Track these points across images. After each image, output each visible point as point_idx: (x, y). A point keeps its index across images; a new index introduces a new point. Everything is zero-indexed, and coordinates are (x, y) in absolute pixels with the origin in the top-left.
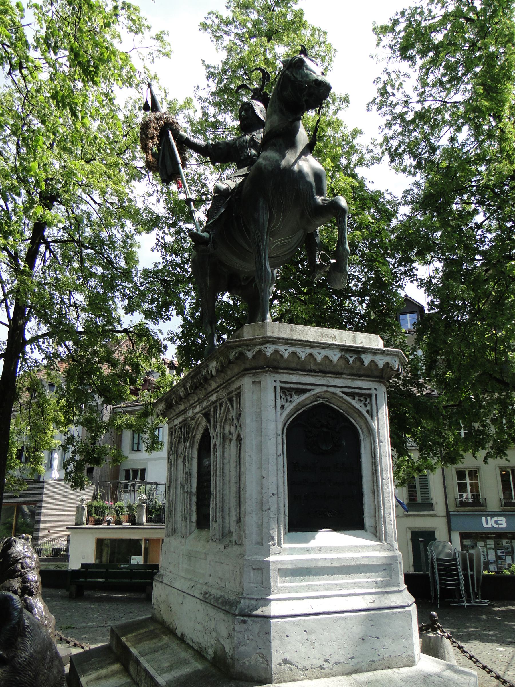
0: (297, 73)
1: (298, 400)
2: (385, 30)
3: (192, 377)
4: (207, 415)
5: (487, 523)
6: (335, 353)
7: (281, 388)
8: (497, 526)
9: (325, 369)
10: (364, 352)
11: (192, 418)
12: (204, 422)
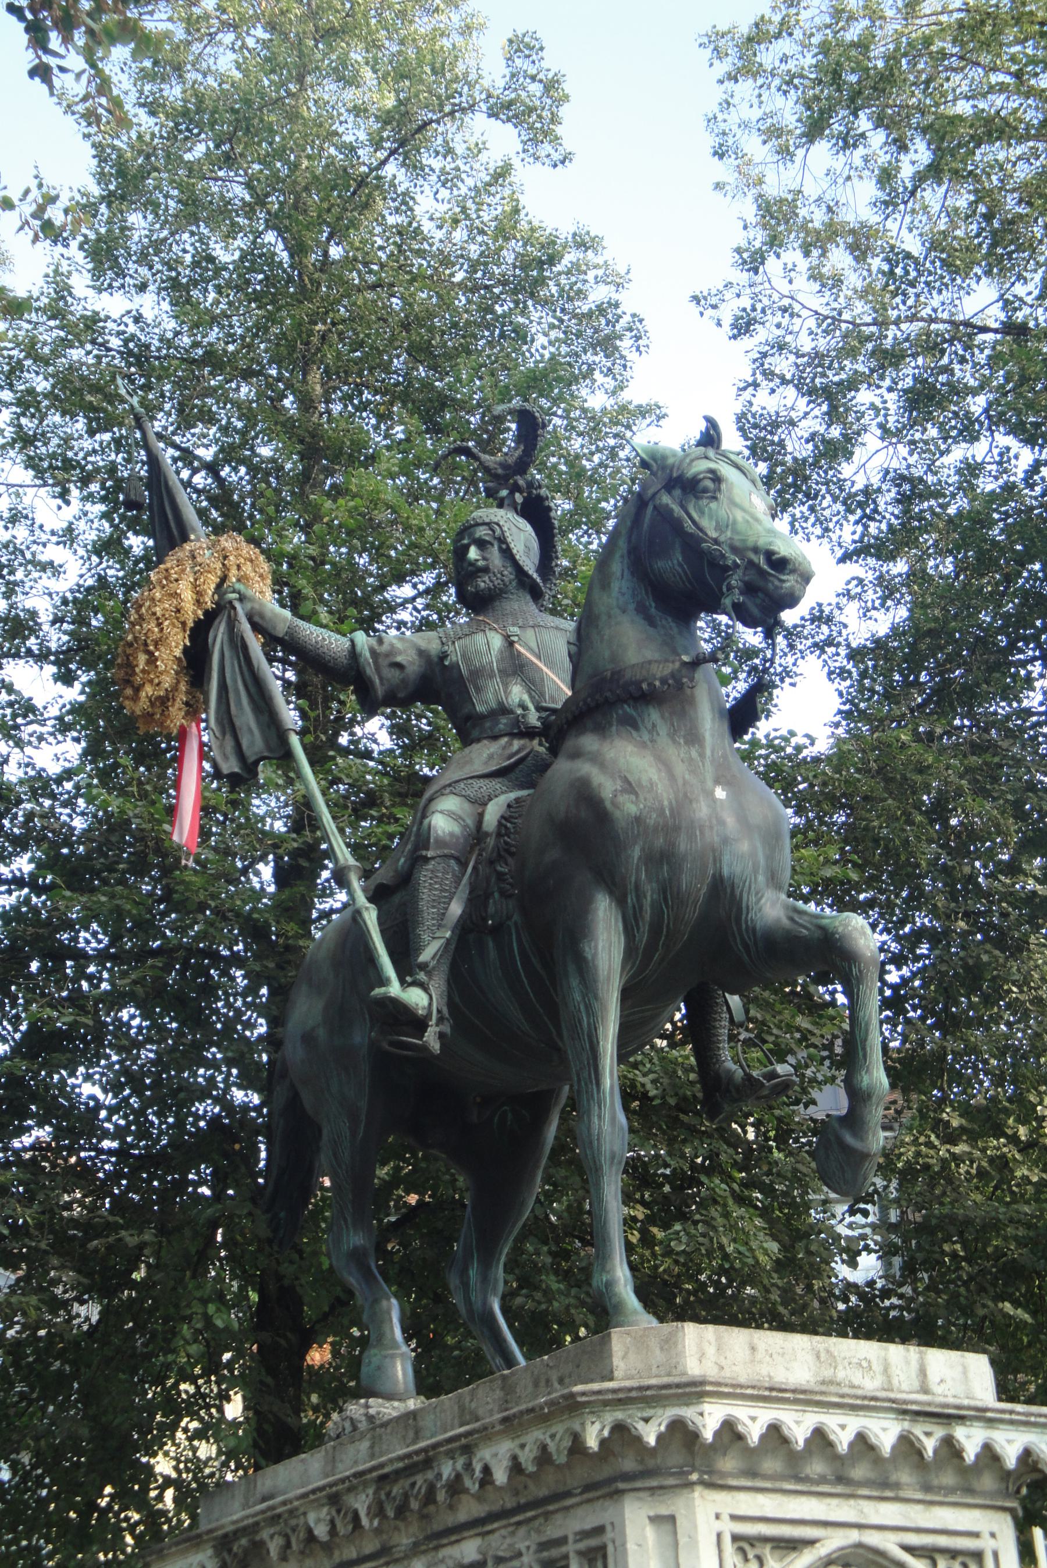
0: (702, 513)
2: (760, 35)
3: (383, 1478)
6: (886, 1423)
7: (736, 1538)
10: (961, 1419)
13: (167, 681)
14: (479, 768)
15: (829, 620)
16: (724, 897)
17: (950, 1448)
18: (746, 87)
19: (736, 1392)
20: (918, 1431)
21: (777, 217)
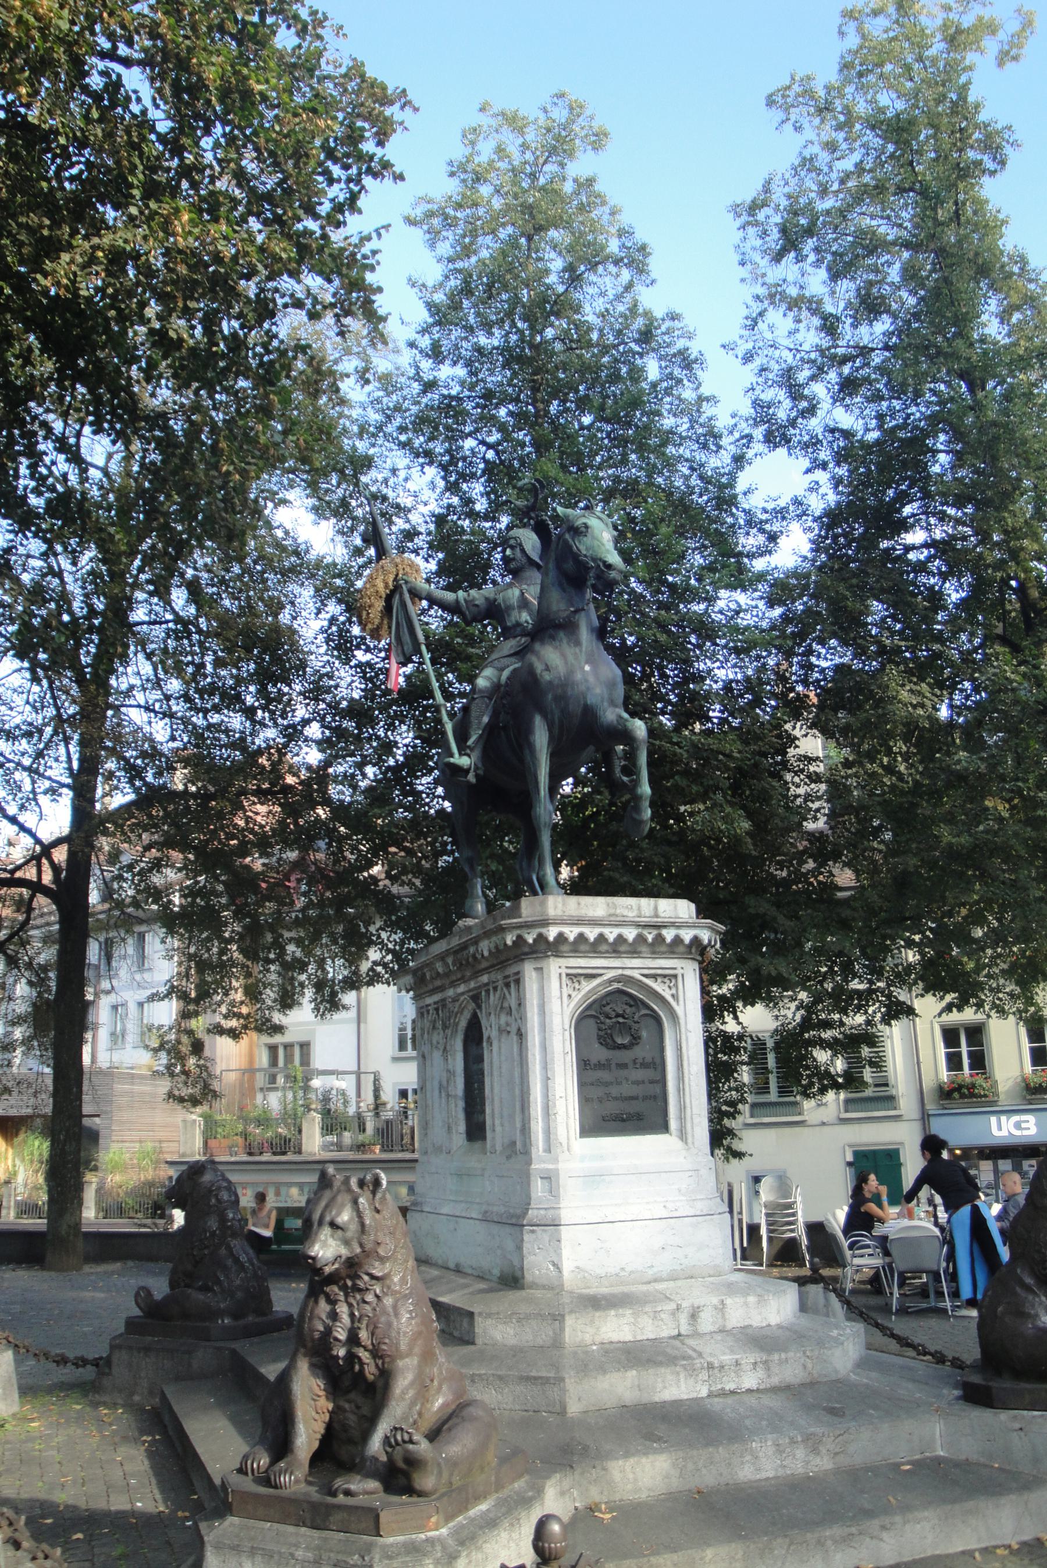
1: (587, 986)
2: (754, 207)
4: (476, 998)
5: (1000, 1128)
8: (1018, 1133)
9: (618, 947)
11: (455, 1000)
12: (472, 1006)
13: (377, 621)
14: (506, 652)
15: (801, 504)
16: (589, 713)
17: (660, 939)
18: (751, 231)
19: (563, 923)
20: (645, 932)
21: (775, 296)
